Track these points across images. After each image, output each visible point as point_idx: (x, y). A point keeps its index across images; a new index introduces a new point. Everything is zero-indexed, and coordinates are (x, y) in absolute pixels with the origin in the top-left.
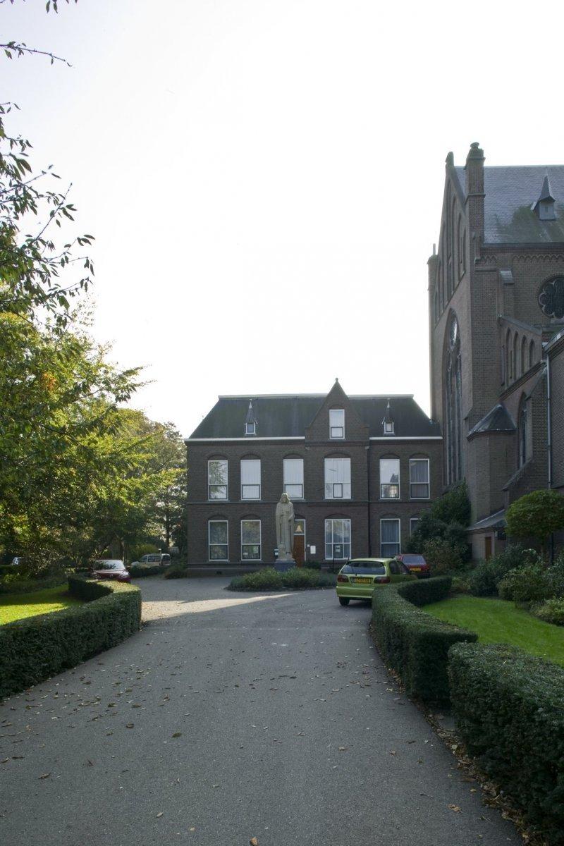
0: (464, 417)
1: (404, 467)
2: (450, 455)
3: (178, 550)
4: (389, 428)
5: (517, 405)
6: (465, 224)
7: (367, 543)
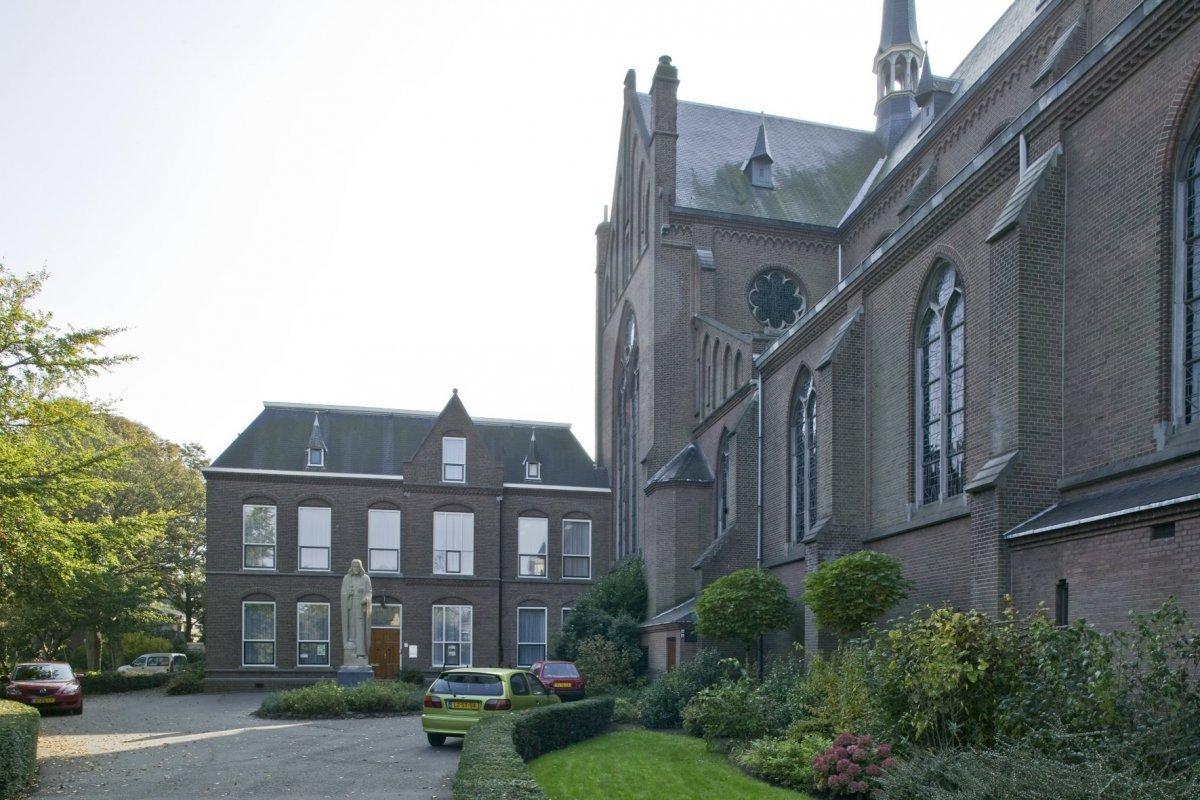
0: (642, 459)
1: (554, 533)
2: (621, 516)
3: (204, 648)
4: (533, 470)
5: (717, 446)
6: (650, 177)
7: (497, 647)
